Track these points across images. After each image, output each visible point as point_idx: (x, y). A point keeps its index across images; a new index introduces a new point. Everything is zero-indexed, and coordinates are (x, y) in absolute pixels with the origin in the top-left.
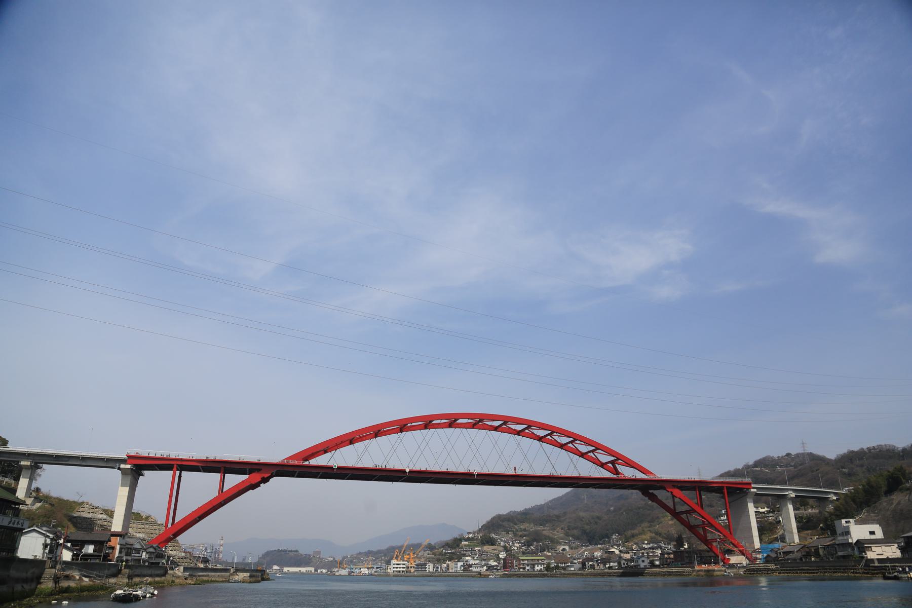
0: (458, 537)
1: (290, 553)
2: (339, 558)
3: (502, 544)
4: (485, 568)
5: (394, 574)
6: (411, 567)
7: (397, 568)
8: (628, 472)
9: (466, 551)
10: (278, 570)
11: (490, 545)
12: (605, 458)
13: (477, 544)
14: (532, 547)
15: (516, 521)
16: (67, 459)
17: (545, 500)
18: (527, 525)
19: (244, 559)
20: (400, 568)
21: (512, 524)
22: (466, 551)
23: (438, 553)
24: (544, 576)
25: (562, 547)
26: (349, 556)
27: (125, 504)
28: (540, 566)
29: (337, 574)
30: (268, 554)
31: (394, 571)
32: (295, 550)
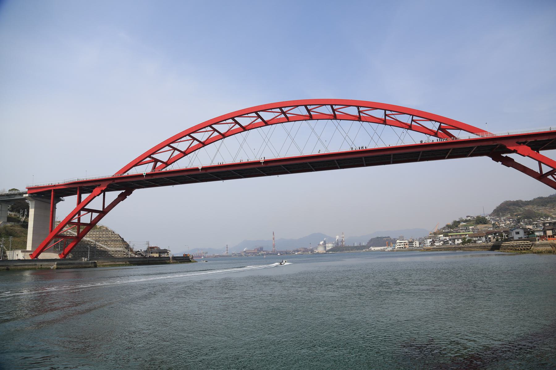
0: (458, 220)
1: (384, 239)
3: (493, 222)
5: (398, 249)
7: (400, 245)
8: (462, 135)
11: (483, 224)
12: (434, 126)
13: (472, 224)
15: (521, 205)
16: (14, 196)
21: (517, 207)
22: (462, 230)
23: (438, 233)
24: (460, 248)
27: (33, 220)
29: (386, 250)
31: (398, 248)
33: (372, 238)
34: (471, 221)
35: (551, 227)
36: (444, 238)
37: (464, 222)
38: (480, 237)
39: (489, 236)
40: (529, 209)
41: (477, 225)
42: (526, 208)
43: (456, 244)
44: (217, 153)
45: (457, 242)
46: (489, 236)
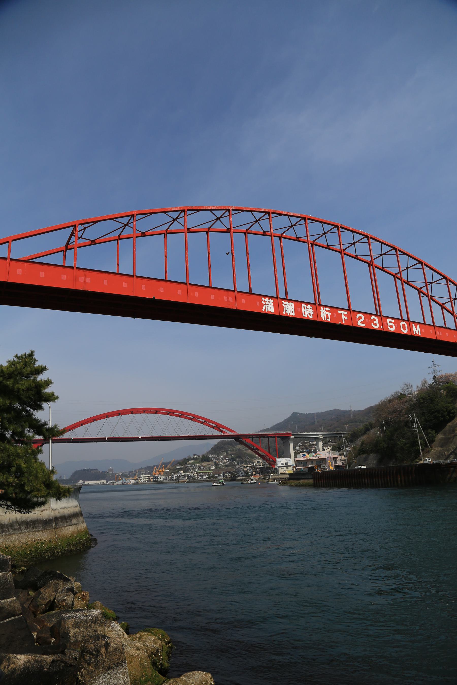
0: (187, 458)
1: (92, 471)
2: (126, 472)
3: (214, 461)
4: (187, 477)
6: (151, 478)
7: (144, 479)
9: (190, 466)
10: (82, 483)
14: (235, 462)
15: (234, 444)
17: (418, 387)
18: (241, 447)
19: (60, 477)
20: (146, 479)
21: (231, 447)
22: (190, 466)
23: (172, 469)
25: (257, 460)
26: (133, 471)
28: (206, 476)
29: (115, 484)
30: (76, 473)
31: (142, 481)
32: (95, 469)
33: (77, 470)
34: (197, 459)
35: (255, 470)
36: (185, 474)
37: (192, 460)
38: (218, 474)
39: (226, 474)
40: (240, 449)
41: (202, 463)
42: (237, 448)
43: (204, 478)
44: (112, 432)
45: (204, 477)
46: (226, 474)
